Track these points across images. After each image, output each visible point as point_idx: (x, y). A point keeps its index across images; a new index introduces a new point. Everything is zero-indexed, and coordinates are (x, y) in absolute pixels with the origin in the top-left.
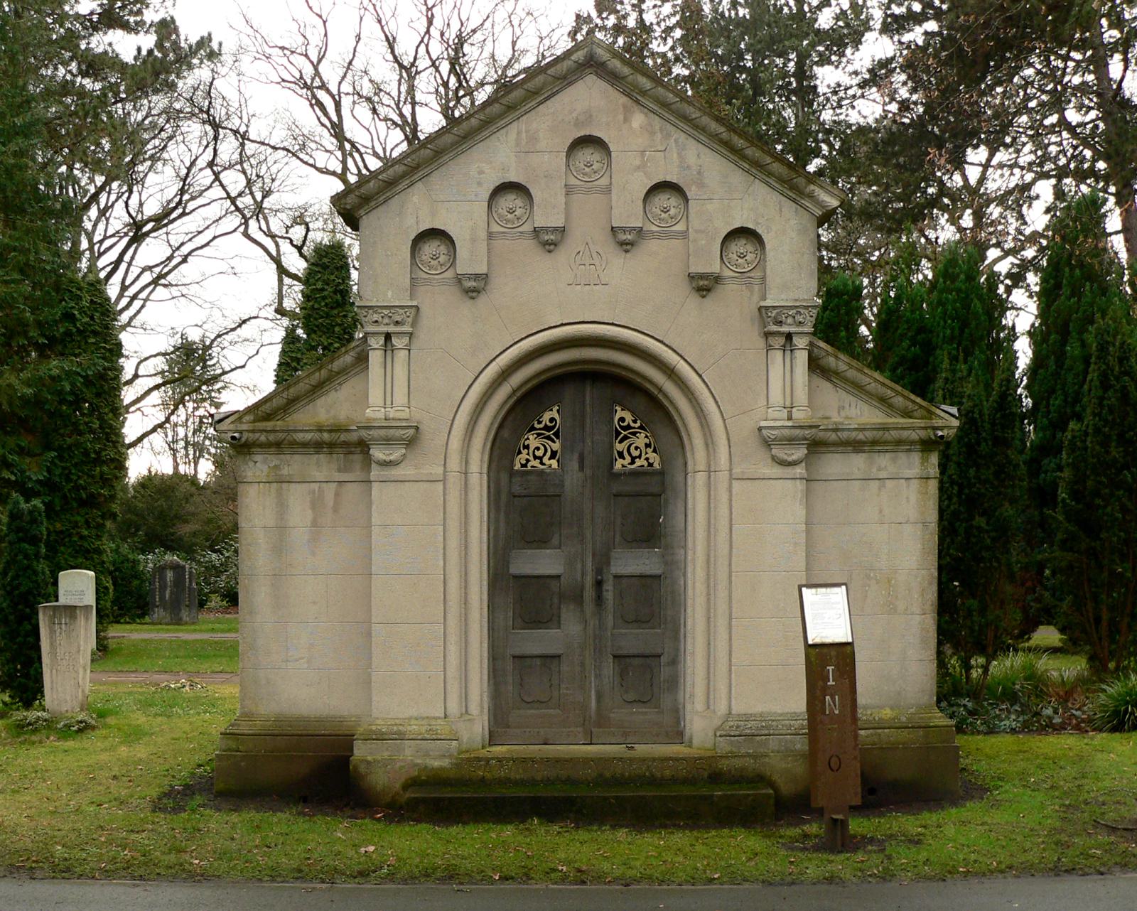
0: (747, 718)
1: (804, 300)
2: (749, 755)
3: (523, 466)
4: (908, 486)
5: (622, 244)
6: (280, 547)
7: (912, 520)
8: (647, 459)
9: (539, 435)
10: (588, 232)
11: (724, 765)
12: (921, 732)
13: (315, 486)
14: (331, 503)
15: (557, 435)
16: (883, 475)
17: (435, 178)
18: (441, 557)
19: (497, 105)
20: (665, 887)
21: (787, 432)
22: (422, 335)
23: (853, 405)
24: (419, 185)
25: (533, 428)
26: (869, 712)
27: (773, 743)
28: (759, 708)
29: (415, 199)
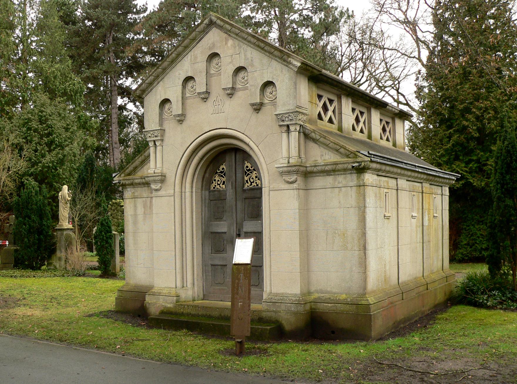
0: (277, 295)
1: (292, 109)
2: (273, 311)
3: (214, 188)
4: (351, 190)
5: (229, 94)
6: (135, 223)
7: (354, 206)
8: (256, 183)
9: (219, 175)
10: (216, 92)
11: (264, 315)
12: (355, 307)
13: (144, 199)
14: (149, 206)
15: (224, 175)
16: (340, 185)
17: (165, 79)
18: (173, 225)
19: (180, 47)
20: (138, 359)
21: (285, 169)
22: (166, 138)
23: (327, 153)
24: (161, 83)
25: (217, 173)
26: (336, 295)
27: (283, 307)
28: (281, 291)
29: (160, 88)
